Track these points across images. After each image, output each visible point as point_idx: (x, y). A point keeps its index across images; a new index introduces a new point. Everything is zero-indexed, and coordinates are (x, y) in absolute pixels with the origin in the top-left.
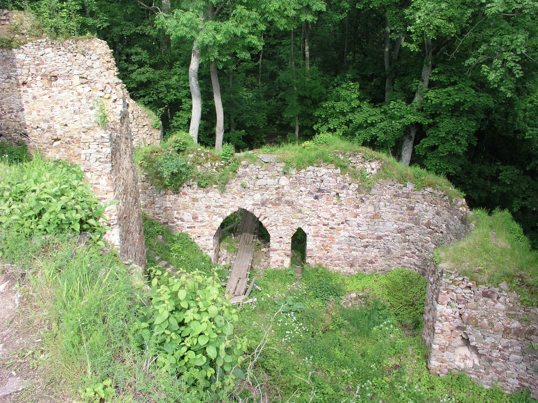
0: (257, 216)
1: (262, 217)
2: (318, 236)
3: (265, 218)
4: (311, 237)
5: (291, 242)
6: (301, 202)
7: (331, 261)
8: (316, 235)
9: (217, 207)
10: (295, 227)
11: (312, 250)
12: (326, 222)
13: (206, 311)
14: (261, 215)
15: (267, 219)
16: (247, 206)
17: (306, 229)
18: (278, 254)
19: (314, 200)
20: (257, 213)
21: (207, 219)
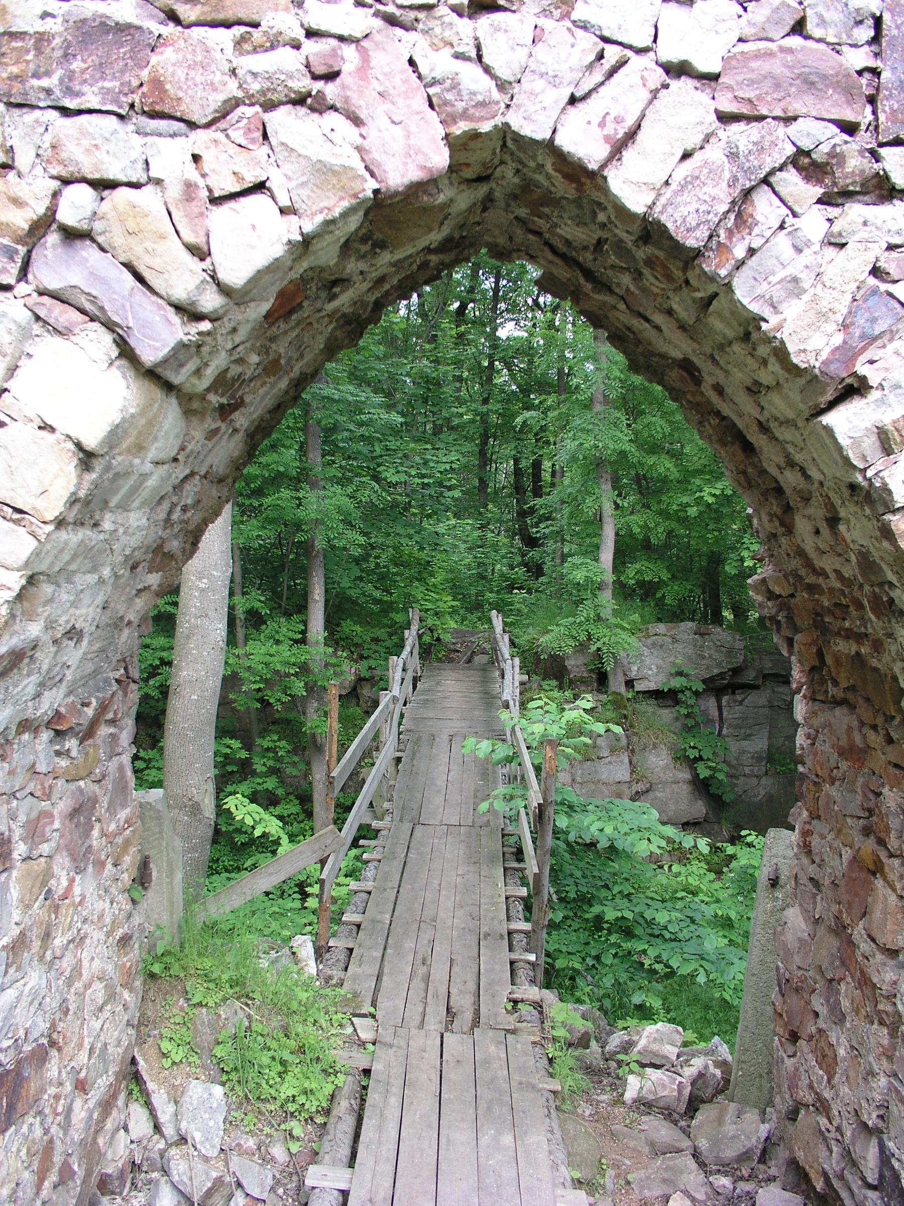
16: (623, 97)
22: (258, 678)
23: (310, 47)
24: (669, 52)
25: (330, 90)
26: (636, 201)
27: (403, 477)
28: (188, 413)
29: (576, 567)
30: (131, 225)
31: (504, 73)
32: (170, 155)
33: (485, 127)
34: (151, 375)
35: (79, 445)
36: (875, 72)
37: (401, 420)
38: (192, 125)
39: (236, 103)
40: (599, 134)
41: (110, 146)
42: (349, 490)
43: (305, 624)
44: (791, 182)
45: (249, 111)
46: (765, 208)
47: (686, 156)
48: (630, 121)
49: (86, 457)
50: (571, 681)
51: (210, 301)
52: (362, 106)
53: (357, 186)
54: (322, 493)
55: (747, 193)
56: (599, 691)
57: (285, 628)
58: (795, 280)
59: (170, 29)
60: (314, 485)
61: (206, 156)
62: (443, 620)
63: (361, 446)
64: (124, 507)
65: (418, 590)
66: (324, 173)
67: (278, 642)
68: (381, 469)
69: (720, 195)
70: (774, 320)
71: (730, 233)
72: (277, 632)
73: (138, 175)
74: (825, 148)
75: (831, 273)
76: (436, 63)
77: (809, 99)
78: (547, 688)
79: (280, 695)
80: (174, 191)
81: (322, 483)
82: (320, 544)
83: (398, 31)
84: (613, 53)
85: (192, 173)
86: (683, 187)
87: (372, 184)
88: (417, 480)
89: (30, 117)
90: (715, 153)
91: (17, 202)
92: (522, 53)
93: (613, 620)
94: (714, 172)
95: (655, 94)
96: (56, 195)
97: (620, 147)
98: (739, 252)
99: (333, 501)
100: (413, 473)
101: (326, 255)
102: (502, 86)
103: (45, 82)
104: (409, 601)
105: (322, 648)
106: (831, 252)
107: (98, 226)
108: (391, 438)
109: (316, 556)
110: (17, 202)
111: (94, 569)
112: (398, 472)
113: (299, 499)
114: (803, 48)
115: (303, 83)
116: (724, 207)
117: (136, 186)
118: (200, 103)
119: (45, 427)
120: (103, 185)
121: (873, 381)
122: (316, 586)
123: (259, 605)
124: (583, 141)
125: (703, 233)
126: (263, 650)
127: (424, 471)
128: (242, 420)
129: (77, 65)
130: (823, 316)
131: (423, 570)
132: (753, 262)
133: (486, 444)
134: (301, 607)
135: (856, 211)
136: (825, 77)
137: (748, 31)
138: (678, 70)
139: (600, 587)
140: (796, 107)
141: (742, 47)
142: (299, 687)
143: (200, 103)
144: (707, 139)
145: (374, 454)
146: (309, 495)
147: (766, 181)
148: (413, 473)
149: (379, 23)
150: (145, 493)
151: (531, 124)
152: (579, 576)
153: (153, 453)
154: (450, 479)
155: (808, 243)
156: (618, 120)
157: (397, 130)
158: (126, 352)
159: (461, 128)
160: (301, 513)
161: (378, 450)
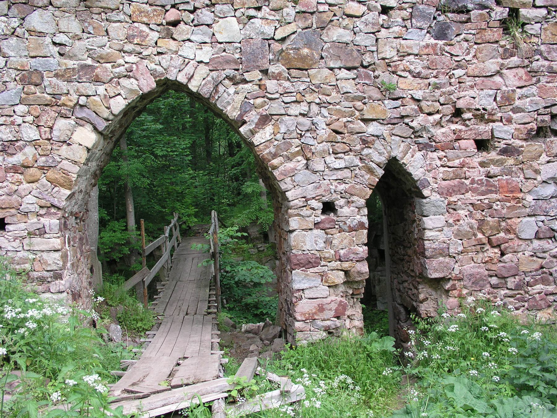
0: (232, 113)
1: (253, 117)
2: (461, 190)
3: (265, 120)
4: (435, 197)
5: (365, 220)
6: (389, 53)
7: (518, 287)
8: (457, 184)
9: (63, 75)
10: (378, 156)
11: (444, 252)
12: (484, 129)
13: (359, 208)
14: (246, 107)
15: (269, 129)
16: (189, 69)
17: (416, 165)
18: (322, 275)
19: (433, 41)
20: (230, 101)
21: (30, 133)
22: (108, 247)
23: (127, 65)
24: (198, 59)
25: (131, 74)
26: (194, 90)
27: (165, 153)
28: (104, 139)
29: (248, 186)
30: (94, 104)
31: (165, 67)
32: (101, 90)
33: (163, 78)
34: (100, 133)
35: (87, 148)
36: (241, 58)
37: (161, 126)
38: (104, 83)
39: (113, 78)
40: (185, 77)
41: (90, 88)
42: (141, 160)
43: (127, 223)
44: (227, 82)
45: (116, 80)
46: (221, 89)
47: (204, 79)
48: (191, 74)
49: (88, 150)
50: (251, 239)
51: (111, 117)
52: (138, 76)
53: (138, 93)
54: (129, 162)
55: (217, 86)
56: (265, 243)
57: (116, 225)
58: (228, 102)
59: (98, 65)
60: (125, 160)
61: (108, 89)
62: (190, 218)
63: (145, 140)
64: (92, 161)
65: (177, 205)
66: (132, 91)
67: (115, 231)
68: (155, 150)
69: (211, 87)
70: (225, 110)
71: (214, 93)
72: (114, 227)
73: (95, 94)
74: (232, 75)
75: (236, 99)
76: (152, 66)
77: (228, 65)
78: (241, 243)
79: (118, 255)
80: (102, 97)
81: (128, 158)
82: (130, 185)
83: (144, 60)
84: (186, 60)
85: (106, 93)
86: (204, 86)
87: (141, 92)
88: (171, 153)
89: (72, 84)
90: (209, 78)
91: (71, 101)
92: (168, 63)
93: (268, 209)
94: (210, 82)
95: (196, 68)
96: (79, 98)
97: (189, 80)
98: (216, 98)
99: (134, 165)
100: (169, 150)
101: (133, 104)
102: (165, 70)
103: (75, 77)
104: (174, 209)
105: (135, 232)
106: (236, 95)
107: (87, 104)
108: (158, 135)
109: (129, 191)
110: (71, 101)
111: (86, 176)
112: (162, 150)
113: (119, 166)
114: (225, 56)
115: (125, 74)
116: (212, 89)
117: (94, 96)
118: (106, 78)
119: (80, 145)
120: (88, 96)
121: (247, 120)
122: (130, 205)
123: (105, 215)
124: (182, 78)
125: (208, 95)
126: (109, 235)
127: (174, 149)
128: (114, 139)
129: (81, 73)
130: (235, 109)
131: (180, 196)
132: (220, 99)
133: (208, 132)
134: (124, 216)
135: (241, 86)
136: (230, 61)
137: (214, 53)
138: (201, 62)
139: (261, 194)
140: (225, 67)
141: (213, 56)
142: (126, 250)
143: (106, 78)
144: (208, 75)
145: (151, 143)
146: (123, 164)
147: (220, 82)
148: (169, 150)
149: (139, 59)
150: (96, 158)
151: (172, 77)
152: (249, 190)
153: (98, 149)
154: (186, 152)
155: (230, 94)
156: (189, 74)
157: (145, 81)
158: (95, 129)
159: (158, 79)
160: (120, 172)
161: (152, 141)
